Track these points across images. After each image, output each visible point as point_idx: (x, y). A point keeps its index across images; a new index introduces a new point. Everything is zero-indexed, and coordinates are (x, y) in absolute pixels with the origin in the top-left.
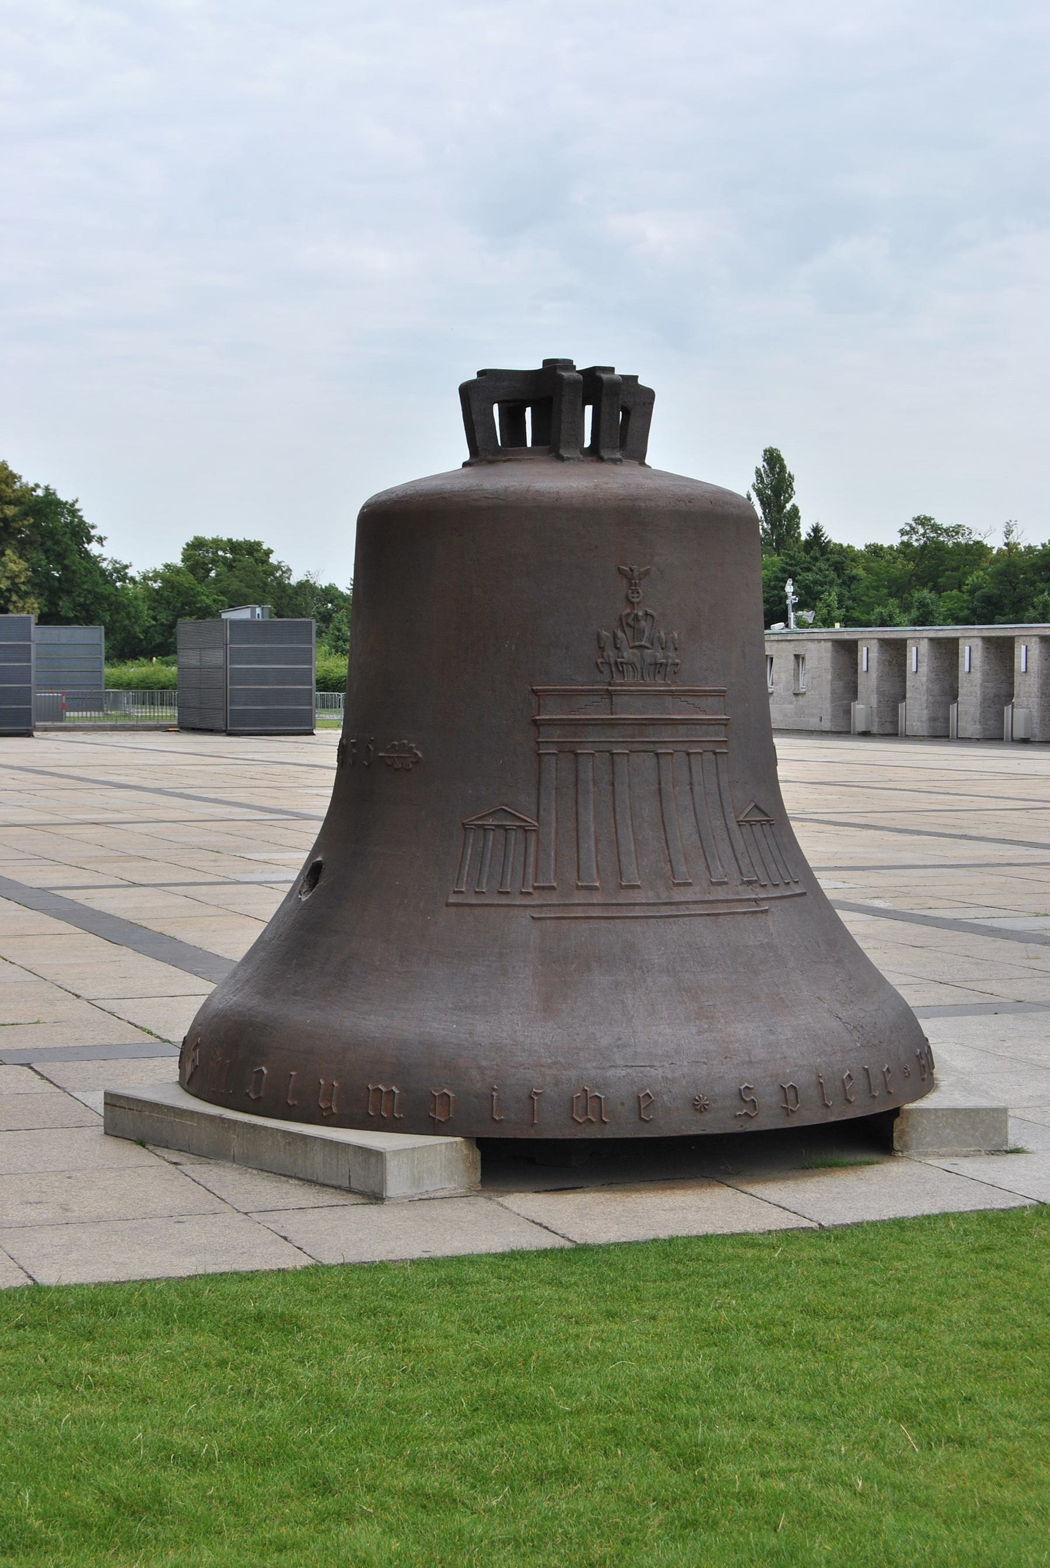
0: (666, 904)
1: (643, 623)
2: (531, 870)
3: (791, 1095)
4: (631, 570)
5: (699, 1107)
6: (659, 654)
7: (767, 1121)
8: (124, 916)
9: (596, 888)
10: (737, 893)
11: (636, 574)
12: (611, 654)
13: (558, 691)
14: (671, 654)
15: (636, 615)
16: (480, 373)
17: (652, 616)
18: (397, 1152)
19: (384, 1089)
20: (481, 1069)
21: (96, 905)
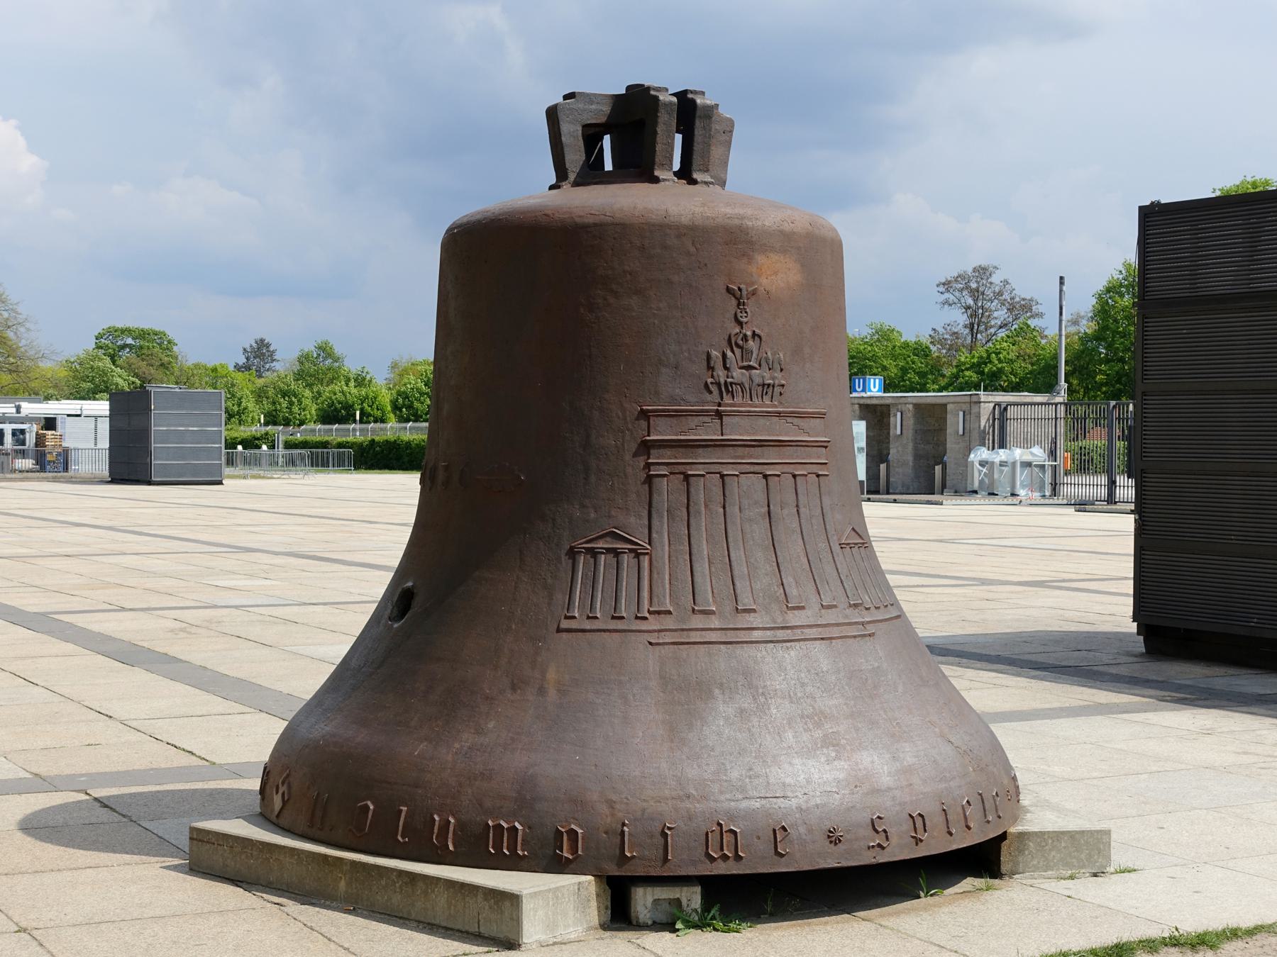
0: (783, 628)
1: (751, 342)
2: (645, 594)
3: (919, 822)
4: (740, 289)
5: (833, 838)
6: (767, 374)
7: (899, 850)
8: (54, 640)
9: (712, 613)
10: (847, 617)
11: (744, 293)
12: (721, 374)
13: (668, 411)
14: (778, 374)
15: (745, 336)
16: (628, 88)
17: (759, 337)
18: (534, 895)
19: (505, 825)
20: (611, 804)
21: (95, 628)
